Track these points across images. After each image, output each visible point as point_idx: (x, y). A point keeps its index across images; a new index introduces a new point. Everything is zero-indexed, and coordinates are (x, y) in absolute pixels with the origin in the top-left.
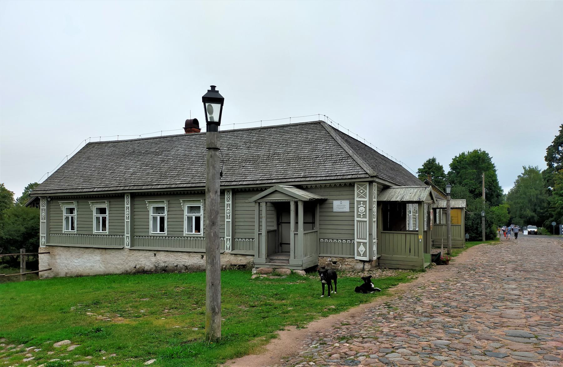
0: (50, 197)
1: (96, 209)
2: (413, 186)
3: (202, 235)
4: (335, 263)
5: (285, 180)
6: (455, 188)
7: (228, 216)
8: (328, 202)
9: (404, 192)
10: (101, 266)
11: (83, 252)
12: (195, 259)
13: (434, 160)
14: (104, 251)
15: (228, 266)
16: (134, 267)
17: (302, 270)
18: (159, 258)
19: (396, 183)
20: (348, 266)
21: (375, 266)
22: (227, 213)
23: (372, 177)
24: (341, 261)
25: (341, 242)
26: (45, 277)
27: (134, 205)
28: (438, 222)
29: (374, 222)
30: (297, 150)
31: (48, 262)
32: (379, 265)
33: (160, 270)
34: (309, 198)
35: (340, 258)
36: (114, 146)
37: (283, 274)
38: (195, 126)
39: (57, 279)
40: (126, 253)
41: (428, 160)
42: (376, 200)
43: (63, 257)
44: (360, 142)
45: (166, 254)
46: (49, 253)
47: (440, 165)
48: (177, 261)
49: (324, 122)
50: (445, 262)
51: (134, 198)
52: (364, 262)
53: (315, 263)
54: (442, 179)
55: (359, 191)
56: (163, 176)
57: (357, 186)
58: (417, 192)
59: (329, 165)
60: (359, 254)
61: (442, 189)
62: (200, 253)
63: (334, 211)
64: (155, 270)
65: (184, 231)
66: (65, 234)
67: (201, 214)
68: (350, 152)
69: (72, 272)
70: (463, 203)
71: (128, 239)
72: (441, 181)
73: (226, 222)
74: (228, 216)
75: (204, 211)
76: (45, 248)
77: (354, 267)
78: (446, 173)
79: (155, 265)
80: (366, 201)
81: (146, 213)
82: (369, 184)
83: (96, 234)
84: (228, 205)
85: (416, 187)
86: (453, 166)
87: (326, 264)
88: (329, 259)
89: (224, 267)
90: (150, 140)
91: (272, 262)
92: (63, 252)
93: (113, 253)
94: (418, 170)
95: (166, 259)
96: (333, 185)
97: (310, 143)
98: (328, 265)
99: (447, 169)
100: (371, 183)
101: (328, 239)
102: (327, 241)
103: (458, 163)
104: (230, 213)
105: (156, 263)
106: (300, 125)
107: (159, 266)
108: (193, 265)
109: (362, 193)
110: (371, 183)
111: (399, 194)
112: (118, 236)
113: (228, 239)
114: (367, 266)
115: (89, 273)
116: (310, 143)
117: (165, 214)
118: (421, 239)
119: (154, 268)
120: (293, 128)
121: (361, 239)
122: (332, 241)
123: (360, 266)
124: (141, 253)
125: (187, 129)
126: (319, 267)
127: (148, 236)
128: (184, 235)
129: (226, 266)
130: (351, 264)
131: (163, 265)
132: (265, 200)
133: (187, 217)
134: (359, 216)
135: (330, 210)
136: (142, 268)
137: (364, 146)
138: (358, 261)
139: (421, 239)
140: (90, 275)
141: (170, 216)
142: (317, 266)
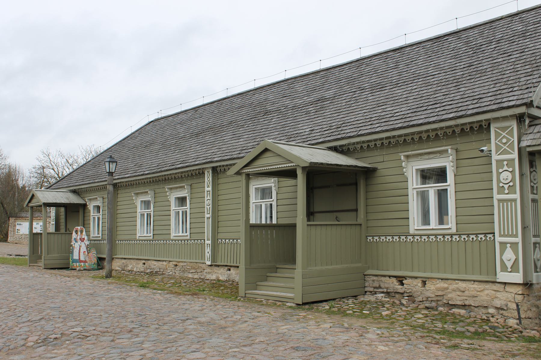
1: (255, 190)
8: (378, 173)
22: (207, 205)
55: (500, 141)
71: (208, 247)
73: (206, 218)
83: (141, 238)
84: (208, 193)
96: (449, 133)
134: (501, 190)
137: (239, 100)
141: (194, 211)
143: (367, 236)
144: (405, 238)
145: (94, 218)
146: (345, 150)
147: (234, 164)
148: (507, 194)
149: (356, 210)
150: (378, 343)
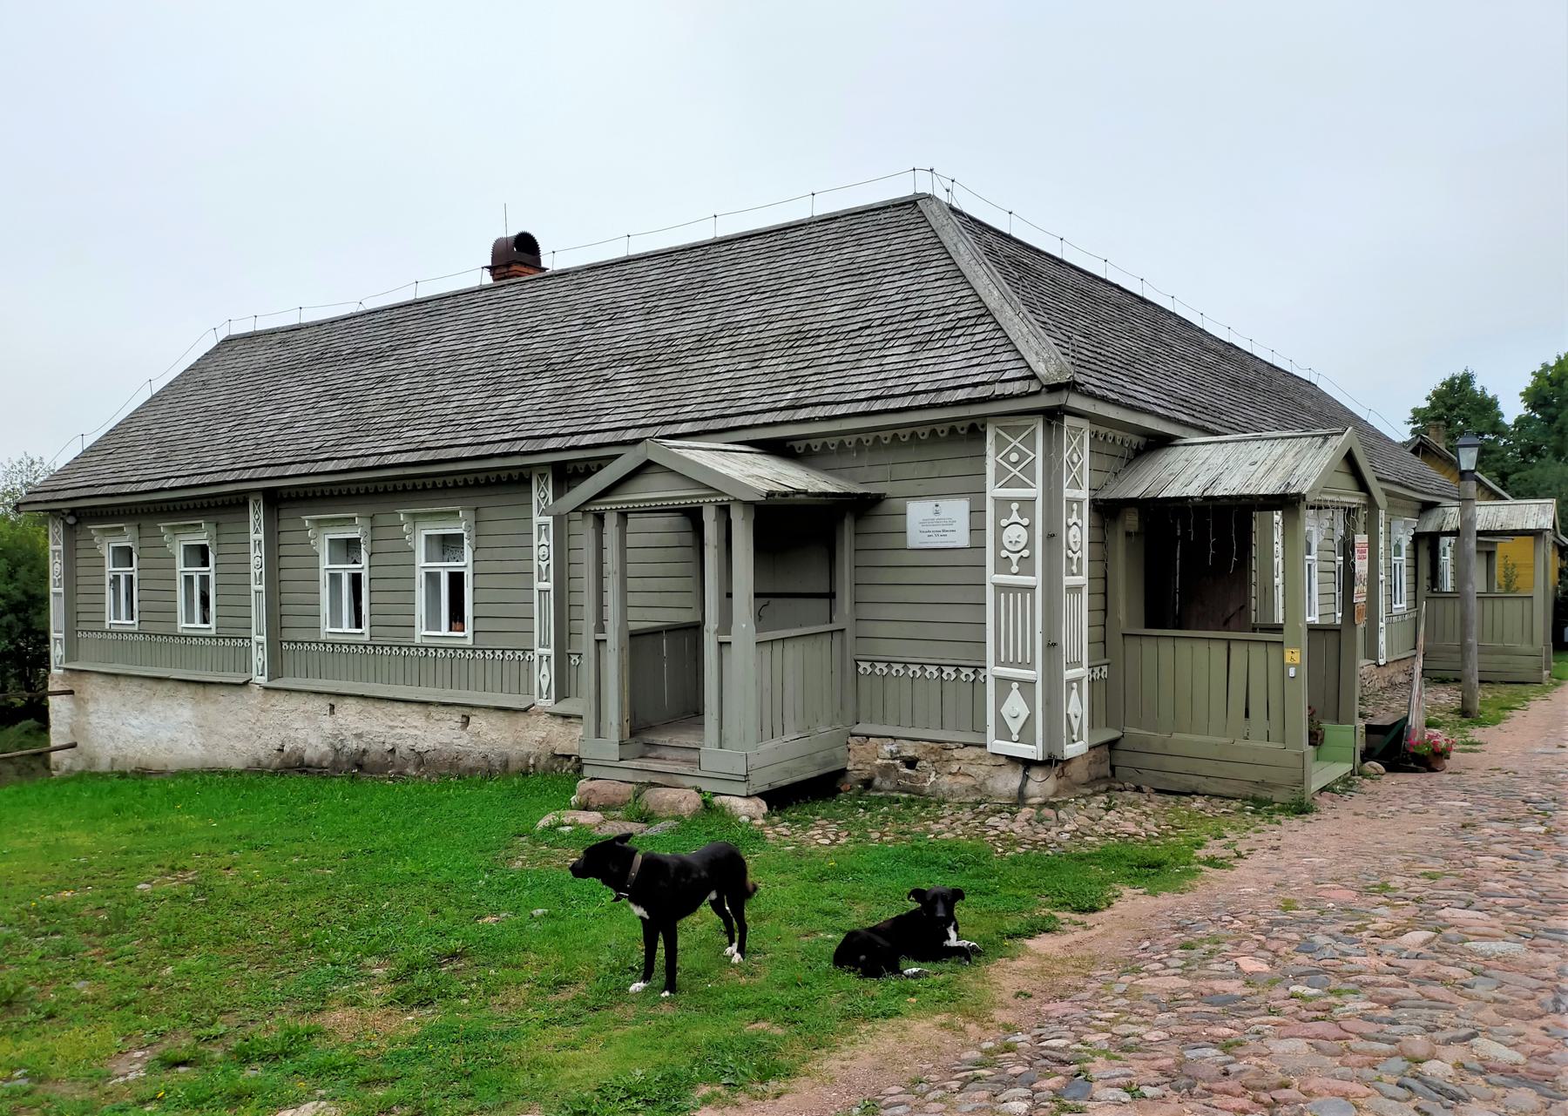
0: (73, 511)
2: (1276, 434)
3: (469, 642)
4: (911, 763)
5: (721, 424)
6: (1541, 471)
7: (544, 569)
9: (1227, 460)
10: (195, 742)
11: (151, 693)
12: (445, 726)
13: (1467, 379)
14: (200, 689)
15: (543, 760)
16: (279, 750)
17: (748, 797)
18: (343, 722)
19: (1207, 425)
20: (960, 779)
21: (1084, 777)
22: (539, 559)
23: (1054, 388)
24: (933, 758)
25: (936, 674)
26: (64, 768)
27: (279, 533)
28: (1448, 584)
29: (1077, 589)
30: (806, 307)
31: (70, 721)
32: (1113, 775)
33: (348, 761)
34: (765, 487)
35: (931, 745)
36: (283, 342)
37: (664, 815)
38: (527, 257)
39: (1284, 619)
40: (254, 697)
41: (1447, 379)
42: (1084, 494)
43: (104, 707)
44: (1117, 286)
45: (360, 708)
46: (71, 692)
47: (1490, 394)
48: (394, 732)
49: (929, 197)
50: (1428, 761)
51: (279, 509)
52: (1028, 764)
53: (826, 764)
54: (1496, 441)
55: (1004, 458)
56: (362, 428)
57: (997, 435)
58: (1283, 455)
59: (899, 353)
60: (1004, 732)
61: (1494, 474)
62: (457, 708)
63: (911, 545)
64: (334, 761)
65: (417, 624)
66: (112, 632)
67: (363, 566)
68: (993, 298)
69: (125, 757)
70: (1545, 513)
71: (260, 651)
72: (1492, 447)
74: (544, 569)
75: (474, 552)
76: (62, 678)
77: (983, 783)
78: (1509, 419)
79: (332, 746)
80: (1033, 500)
81: (309, 561)
82: (1048, 426)
83: (185, 632)
84: (543, 527)
85: (1283, 438)
86: (1537, 398)
87: (878, 767)
88: (888, 747)
89: (531, 761)
90: (381, 315)
91: (650, 755)
92: (105, 693)
93: (226, 699)
94: (1411, 415)
95: (363, 727)
97: (855, 279)
98: (886, 770)
99: (1512, 409)
100: (1053, 416)
101: (889, 663)
102: (886, 671)
103: (1551, 385)
104: (548, 558)
105: (336, 736)
106: (843, 216)
107: (346, 750)
108: (440, 750)
109: (1015, 464)
110: (1053, 416)
111: (1205, 467)
112: (240, 641)
113: (545, 658)
114: (1040, 785)
115: (165, 761)
116: (855, 279)
117: (466, 563)
118: (1292, 665)
119: (330, 754)
120: (819, 229)
121: (1011, 665)
122: (902, 672)
123: (1009, 781)
124: (295, 701)
125: (498, 271)
126: (851, 778)
127: (317, 643)
128: (417, 640)
129: (538, 759)
130: (972, 770)
131: (353, 744)
132: (623, 502)
133: (330, 574)
134: (1003, 565)
135: (894, 541)
136: (298, 753)
138: (1002, 761)
139: (1292, 665)
140: (169, 772)
142: (843, 772)
143: (856, 661)
144: (974, 672)
145: (116, 580)
146: (800, 449)
147: (616, 457)
148: (1015, 574)
149: (831, 596)
150: (1283, 1001)
